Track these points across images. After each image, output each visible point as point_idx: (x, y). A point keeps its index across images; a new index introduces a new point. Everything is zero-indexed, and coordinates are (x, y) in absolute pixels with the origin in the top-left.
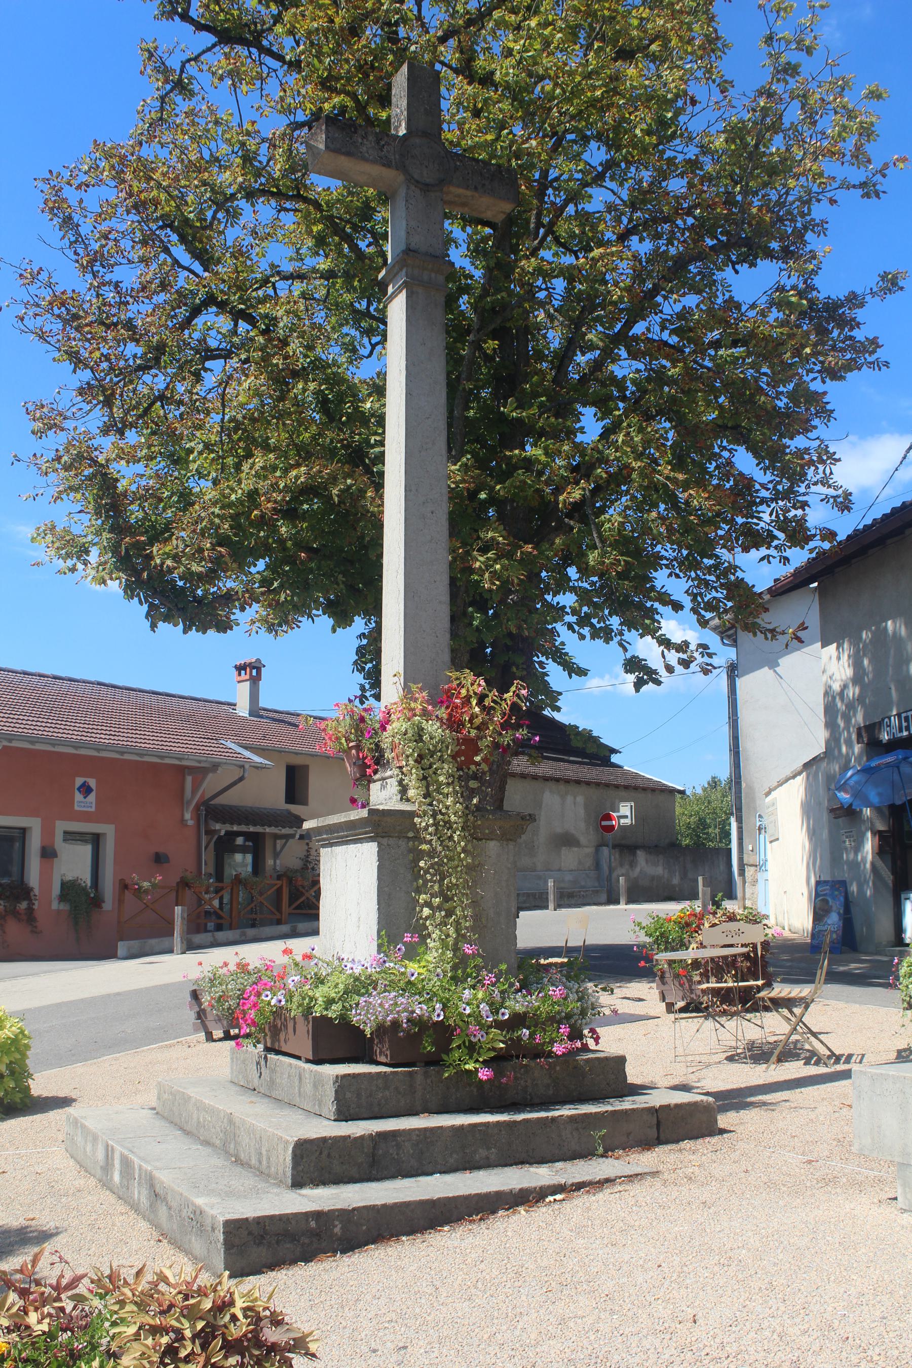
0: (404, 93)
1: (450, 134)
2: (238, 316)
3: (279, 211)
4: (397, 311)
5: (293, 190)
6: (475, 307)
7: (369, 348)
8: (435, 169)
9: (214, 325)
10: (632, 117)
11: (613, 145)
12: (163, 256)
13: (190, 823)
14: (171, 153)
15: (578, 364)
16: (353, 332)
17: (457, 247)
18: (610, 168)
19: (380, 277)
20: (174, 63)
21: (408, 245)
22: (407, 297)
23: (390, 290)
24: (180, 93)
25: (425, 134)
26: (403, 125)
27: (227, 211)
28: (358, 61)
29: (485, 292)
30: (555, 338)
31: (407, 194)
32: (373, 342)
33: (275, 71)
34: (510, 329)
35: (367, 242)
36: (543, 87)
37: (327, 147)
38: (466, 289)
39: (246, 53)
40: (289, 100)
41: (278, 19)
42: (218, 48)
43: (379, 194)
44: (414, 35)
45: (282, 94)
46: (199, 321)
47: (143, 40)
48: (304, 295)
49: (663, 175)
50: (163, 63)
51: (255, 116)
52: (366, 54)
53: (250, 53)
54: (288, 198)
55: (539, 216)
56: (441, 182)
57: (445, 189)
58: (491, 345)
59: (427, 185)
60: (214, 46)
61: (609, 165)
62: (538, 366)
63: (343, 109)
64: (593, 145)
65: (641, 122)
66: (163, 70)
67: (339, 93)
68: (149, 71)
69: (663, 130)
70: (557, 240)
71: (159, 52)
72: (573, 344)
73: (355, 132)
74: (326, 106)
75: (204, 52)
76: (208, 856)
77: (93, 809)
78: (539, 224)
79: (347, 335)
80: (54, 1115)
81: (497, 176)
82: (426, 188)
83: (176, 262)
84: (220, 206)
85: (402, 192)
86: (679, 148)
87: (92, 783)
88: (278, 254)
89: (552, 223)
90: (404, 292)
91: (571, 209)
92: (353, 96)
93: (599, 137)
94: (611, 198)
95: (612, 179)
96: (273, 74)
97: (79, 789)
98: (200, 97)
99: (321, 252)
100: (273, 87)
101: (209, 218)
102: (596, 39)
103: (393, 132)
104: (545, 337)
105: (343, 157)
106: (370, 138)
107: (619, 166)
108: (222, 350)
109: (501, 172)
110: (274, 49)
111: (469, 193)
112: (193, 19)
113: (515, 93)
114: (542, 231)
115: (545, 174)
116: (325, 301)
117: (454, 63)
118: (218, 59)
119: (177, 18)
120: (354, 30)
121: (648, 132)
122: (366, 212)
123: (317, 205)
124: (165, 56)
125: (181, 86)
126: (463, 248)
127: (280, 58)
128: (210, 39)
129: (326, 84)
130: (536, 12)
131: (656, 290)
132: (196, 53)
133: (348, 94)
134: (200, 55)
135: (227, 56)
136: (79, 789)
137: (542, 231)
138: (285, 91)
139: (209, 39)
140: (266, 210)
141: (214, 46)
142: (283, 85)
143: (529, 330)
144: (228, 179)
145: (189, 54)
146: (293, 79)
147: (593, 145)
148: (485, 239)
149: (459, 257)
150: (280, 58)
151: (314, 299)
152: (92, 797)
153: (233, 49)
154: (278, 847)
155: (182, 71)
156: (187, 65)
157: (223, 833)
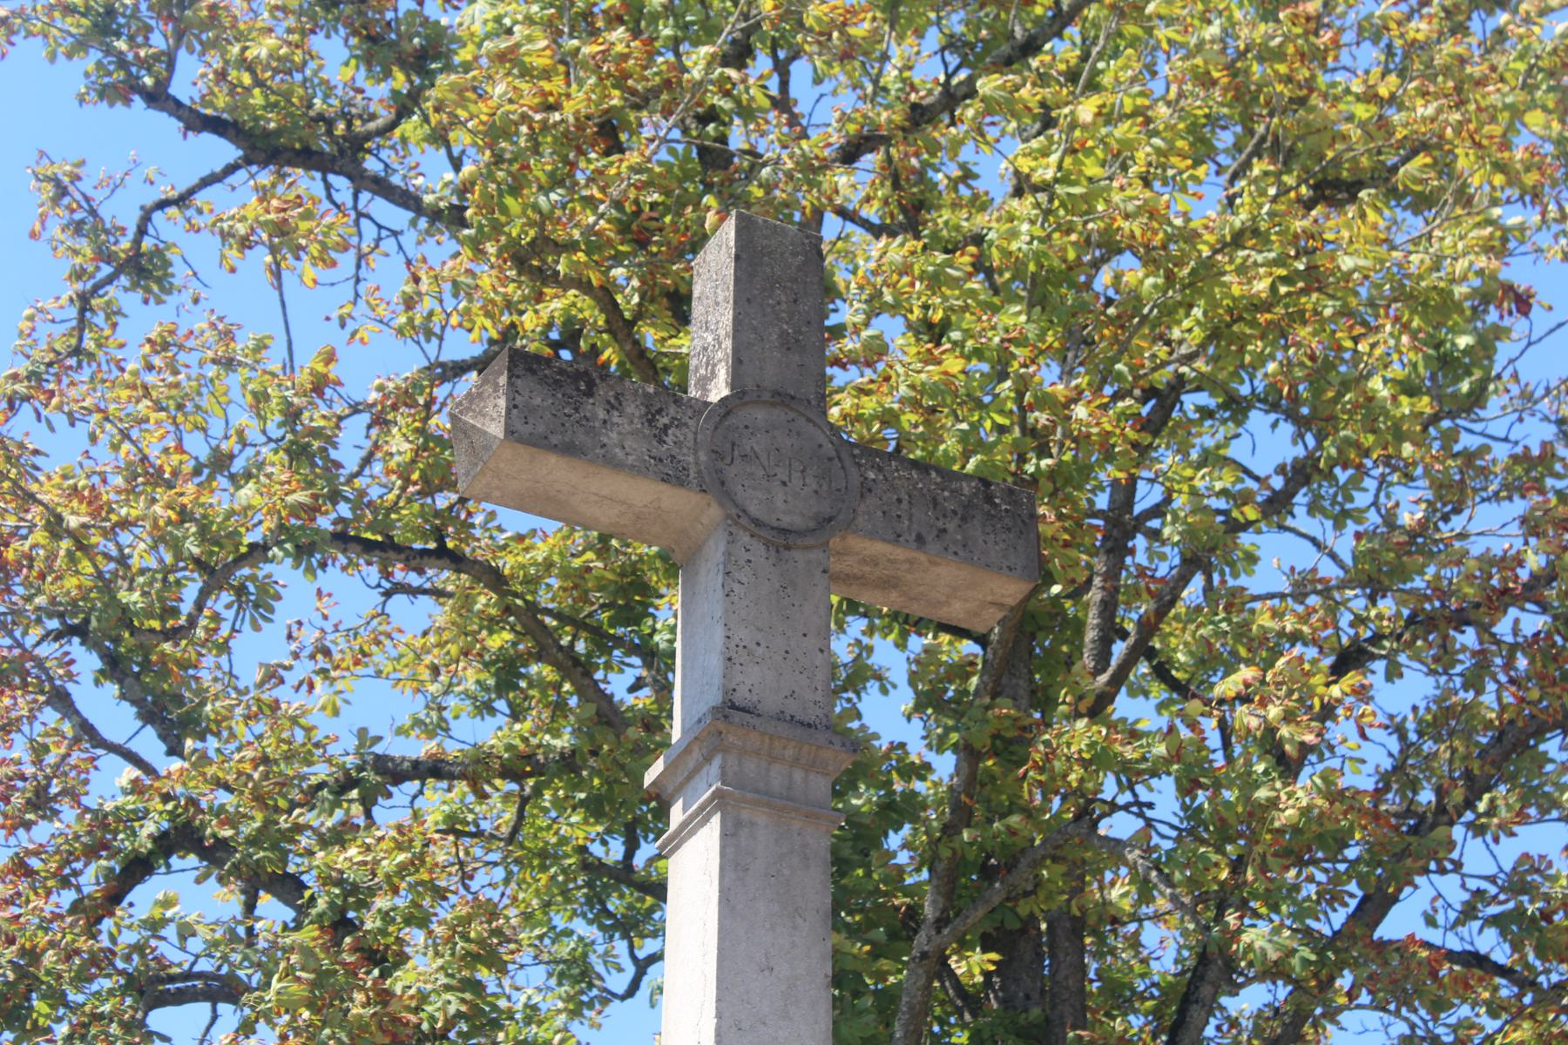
0: (726, 293)
1: (849, 399)
2: (255, 882)
3: (388, 594)
4: (694, 870)
5: (424, 536)
6: (928, 858)
7: (630, 970)
8: (819, 491)
9: (190, 904)
10: (1363, 347)
11: (1311, 419)
12: (50, 716)
14: (93, 438)
15: (1234, 1023)
16: (581, 927)
17: (884, 691)
18: (1307, 481)
19: (649, 777)
20: (122, 211)
21: (729, 692)
22: (725, 835)
23: (677, 815)
24: (135, 286)
25: (781, 398)
26: (722, 373)
27: (241, 591)
28: (618, 205)
29: (961, 815)
30: (1163, 947)
31: (728, 554)
32: (641, 955)
33: (395, 234)
34: (1032, 920)
35: (629, 676)
36: (1117, 277)
37: (510, 432)
38: (897, 810)
39: (318, 189)
40: (428, 303)
41: (405, 106)
42: (241, 175)
43: (663, 557)
44: (769, 146)
45: (409, 288)
46: (144, 898)
47: (42, 154)
48: (453, 827)
49: (1451, 496)
50: (93, 212)
51: (338, 338)
52: (640, 187)
53: (328, 187)
54: (416, 559)
55: (1108, 608)
56: (825, 523)
57: (835, 542)
58: (972, 965)
59: (784, 531)
60: (231, 169)
61: (1301, 474)
62: (1118, 1024)
63: (572, 333)
64: (1258, 420)
65: (1389, 358)
66: (88, 224)
67: (565, 284)
68: (54, 230)
69: (1455, 381)
70: (1162, 672)
71: (85, 186)
72: (1212, 969)
73: (589, 393)
74: (529, 321)
75: (207, 182)
78: (1111, 631)
79: (568, 933)
81: (990, 509)
82: (781, 539)
83: (87, 732)
84: (215, 577)
85: (715, 551)
86: (1498, 428)
88: (374, 710)
89: (1148, 627)
90: (716, 820)
91: (1193, 591)
92: (605, 296)
93: (1271, 401)
94: (1306, 557)
95: (1313, 509)
96: (389, 244)
98: (186, 297)
99: (501, 705)
100: (389, 276)
101: (186, 607)
102: (1257, 153)
103: (693, 392)
104: (1135, 942)
105: (553, 459)
107: (1330, 476)
108: (201, 975)
109: (989, 499)
110: (396, 180)
111: (900, 553)
112: (179, 104)
113: (1043, 287)
114: (1119, 649)
115: (1125, 493)
116: (511, 838)
117: (871, 212)
118: (241, 200)
119: (138, 101)
120: (609, 133)
121: (1409, 388)
122: (632, 596)
123: (495, 579)
124: (98, 196)
125: (145, 269)
126: (904, 698)
127: (407, 199)
128: (223, 151)
129: (532, 262)
130: (1093, 87)
131: (1443, 814)
132: (182, 187)
133: (585, 287)
134: (191, 192)
135: (264, 195)
137: (1119, 649)
138: (417, 280)
139: (219, 151)
140: (350, 590)
141: (231, 169)
142: (410, 261)
143: (1083, 925)
144: (253, 504)
145: (164, 190)
146: (443, 252)
147: (1258, 420)
148: (962, 670)
149: (888, 717)
150: (407, 199)
151: (479, 834)
153: (283, 176)
155: (142, 231)
156: (158, 217)
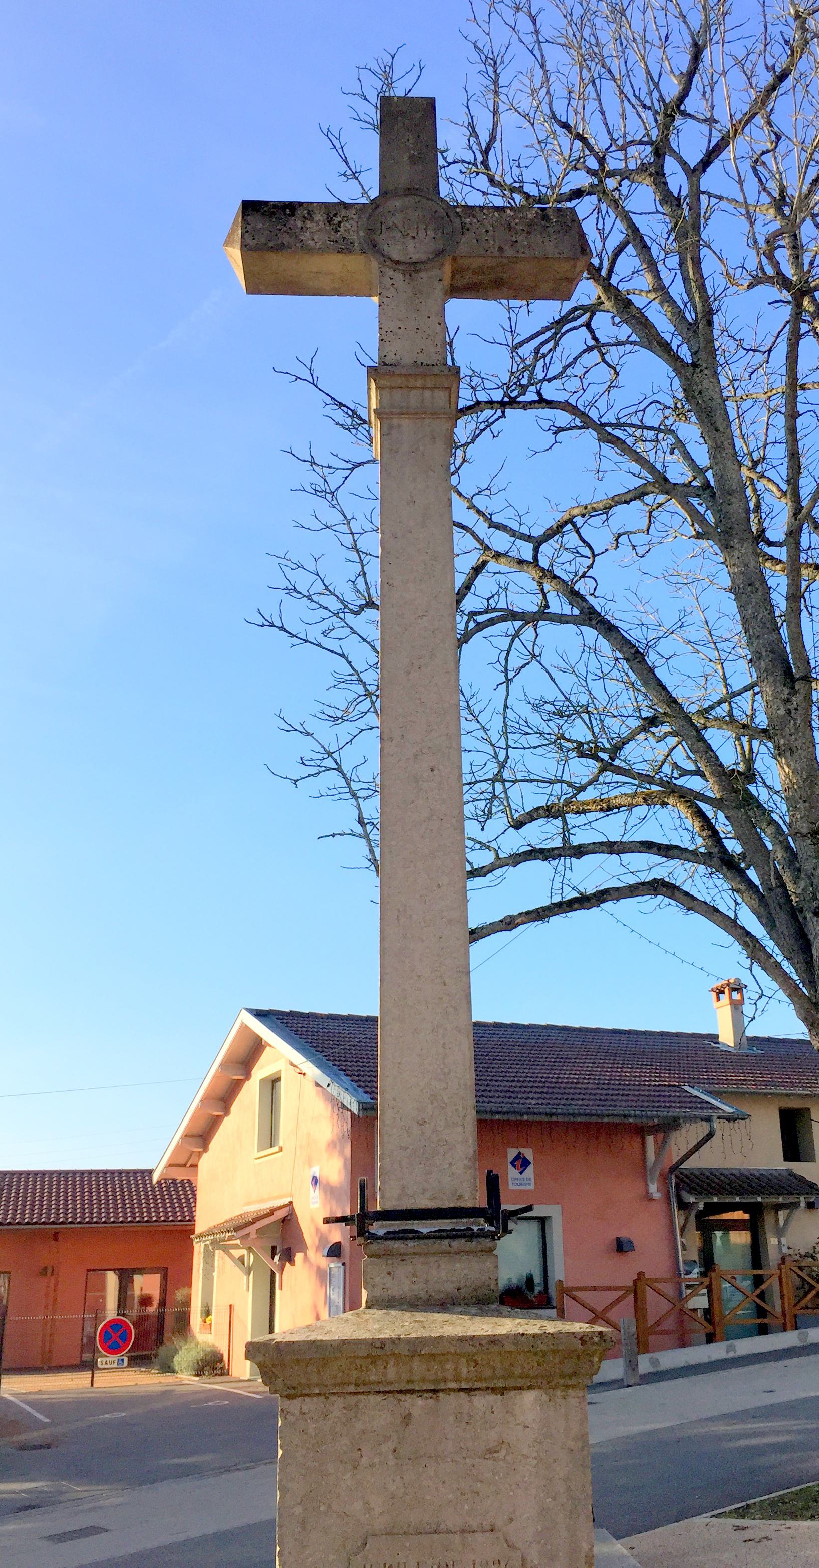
13: (657, 1195)
76: (694, 1239)
77: (532, 1187)
80: (103, 1535)
87: (528, 1153)
97: (513, 1163)
106: (317, 217)
136: (513, 1163)
152: (530, 1171)
154: (782, 1223)
157: (701, 1206)
